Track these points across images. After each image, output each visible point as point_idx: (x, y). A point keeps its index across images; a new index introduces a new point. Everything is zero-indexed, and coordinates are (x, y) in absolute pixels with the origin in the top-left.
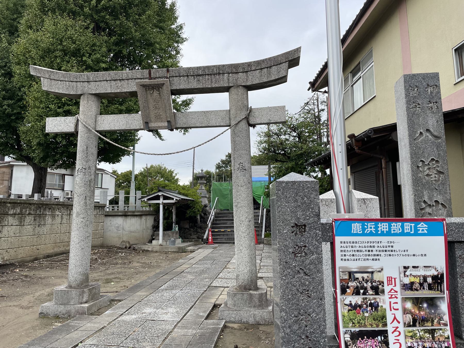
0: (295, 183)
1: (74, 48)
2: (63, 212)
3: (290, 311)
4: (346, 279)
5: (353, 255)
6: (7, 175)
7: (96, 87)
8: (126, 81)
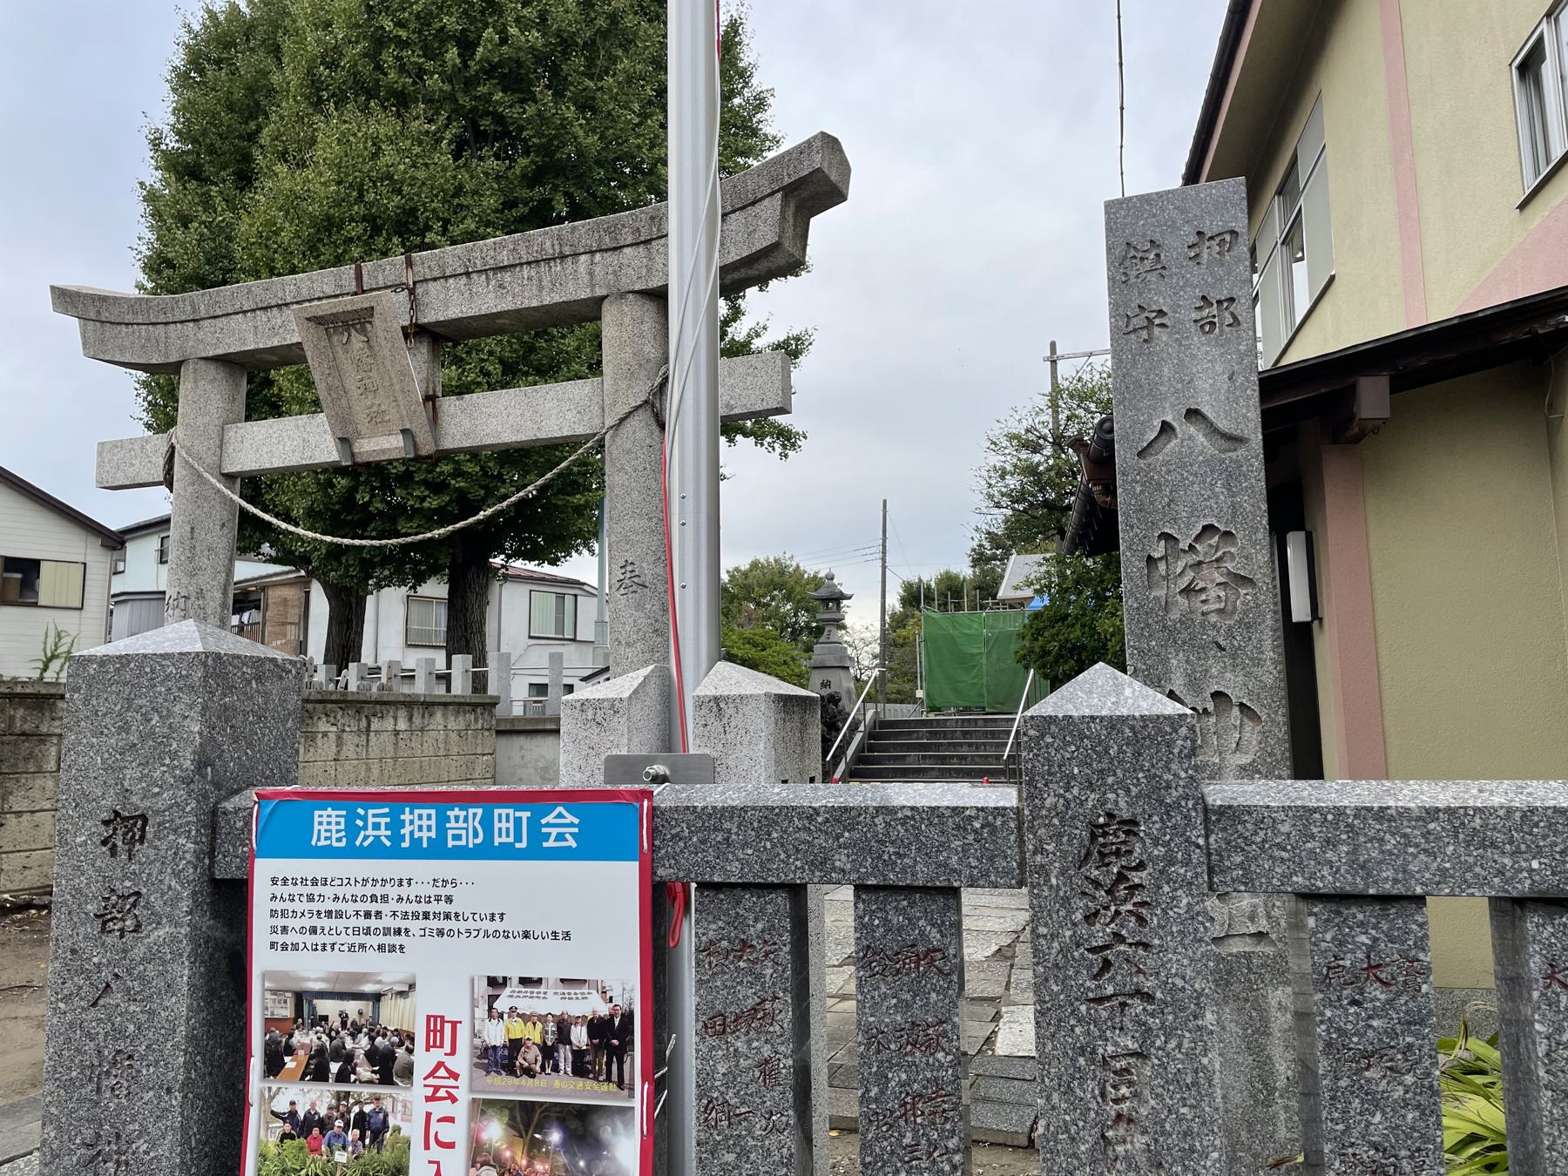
0: (129, 663)
1: (398, 207)
2: (344, 725)
3: (71, 1124)
4: (284, 1020)
5: (313, 930)
6: (293, 607)
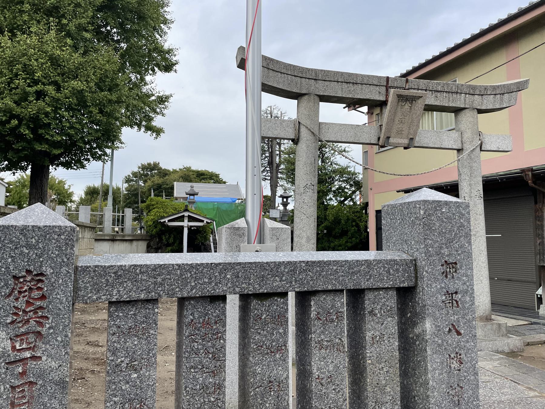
7: (325, 88)
8: (360, 86)
